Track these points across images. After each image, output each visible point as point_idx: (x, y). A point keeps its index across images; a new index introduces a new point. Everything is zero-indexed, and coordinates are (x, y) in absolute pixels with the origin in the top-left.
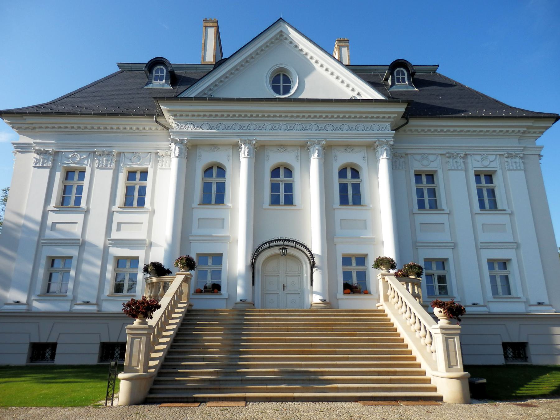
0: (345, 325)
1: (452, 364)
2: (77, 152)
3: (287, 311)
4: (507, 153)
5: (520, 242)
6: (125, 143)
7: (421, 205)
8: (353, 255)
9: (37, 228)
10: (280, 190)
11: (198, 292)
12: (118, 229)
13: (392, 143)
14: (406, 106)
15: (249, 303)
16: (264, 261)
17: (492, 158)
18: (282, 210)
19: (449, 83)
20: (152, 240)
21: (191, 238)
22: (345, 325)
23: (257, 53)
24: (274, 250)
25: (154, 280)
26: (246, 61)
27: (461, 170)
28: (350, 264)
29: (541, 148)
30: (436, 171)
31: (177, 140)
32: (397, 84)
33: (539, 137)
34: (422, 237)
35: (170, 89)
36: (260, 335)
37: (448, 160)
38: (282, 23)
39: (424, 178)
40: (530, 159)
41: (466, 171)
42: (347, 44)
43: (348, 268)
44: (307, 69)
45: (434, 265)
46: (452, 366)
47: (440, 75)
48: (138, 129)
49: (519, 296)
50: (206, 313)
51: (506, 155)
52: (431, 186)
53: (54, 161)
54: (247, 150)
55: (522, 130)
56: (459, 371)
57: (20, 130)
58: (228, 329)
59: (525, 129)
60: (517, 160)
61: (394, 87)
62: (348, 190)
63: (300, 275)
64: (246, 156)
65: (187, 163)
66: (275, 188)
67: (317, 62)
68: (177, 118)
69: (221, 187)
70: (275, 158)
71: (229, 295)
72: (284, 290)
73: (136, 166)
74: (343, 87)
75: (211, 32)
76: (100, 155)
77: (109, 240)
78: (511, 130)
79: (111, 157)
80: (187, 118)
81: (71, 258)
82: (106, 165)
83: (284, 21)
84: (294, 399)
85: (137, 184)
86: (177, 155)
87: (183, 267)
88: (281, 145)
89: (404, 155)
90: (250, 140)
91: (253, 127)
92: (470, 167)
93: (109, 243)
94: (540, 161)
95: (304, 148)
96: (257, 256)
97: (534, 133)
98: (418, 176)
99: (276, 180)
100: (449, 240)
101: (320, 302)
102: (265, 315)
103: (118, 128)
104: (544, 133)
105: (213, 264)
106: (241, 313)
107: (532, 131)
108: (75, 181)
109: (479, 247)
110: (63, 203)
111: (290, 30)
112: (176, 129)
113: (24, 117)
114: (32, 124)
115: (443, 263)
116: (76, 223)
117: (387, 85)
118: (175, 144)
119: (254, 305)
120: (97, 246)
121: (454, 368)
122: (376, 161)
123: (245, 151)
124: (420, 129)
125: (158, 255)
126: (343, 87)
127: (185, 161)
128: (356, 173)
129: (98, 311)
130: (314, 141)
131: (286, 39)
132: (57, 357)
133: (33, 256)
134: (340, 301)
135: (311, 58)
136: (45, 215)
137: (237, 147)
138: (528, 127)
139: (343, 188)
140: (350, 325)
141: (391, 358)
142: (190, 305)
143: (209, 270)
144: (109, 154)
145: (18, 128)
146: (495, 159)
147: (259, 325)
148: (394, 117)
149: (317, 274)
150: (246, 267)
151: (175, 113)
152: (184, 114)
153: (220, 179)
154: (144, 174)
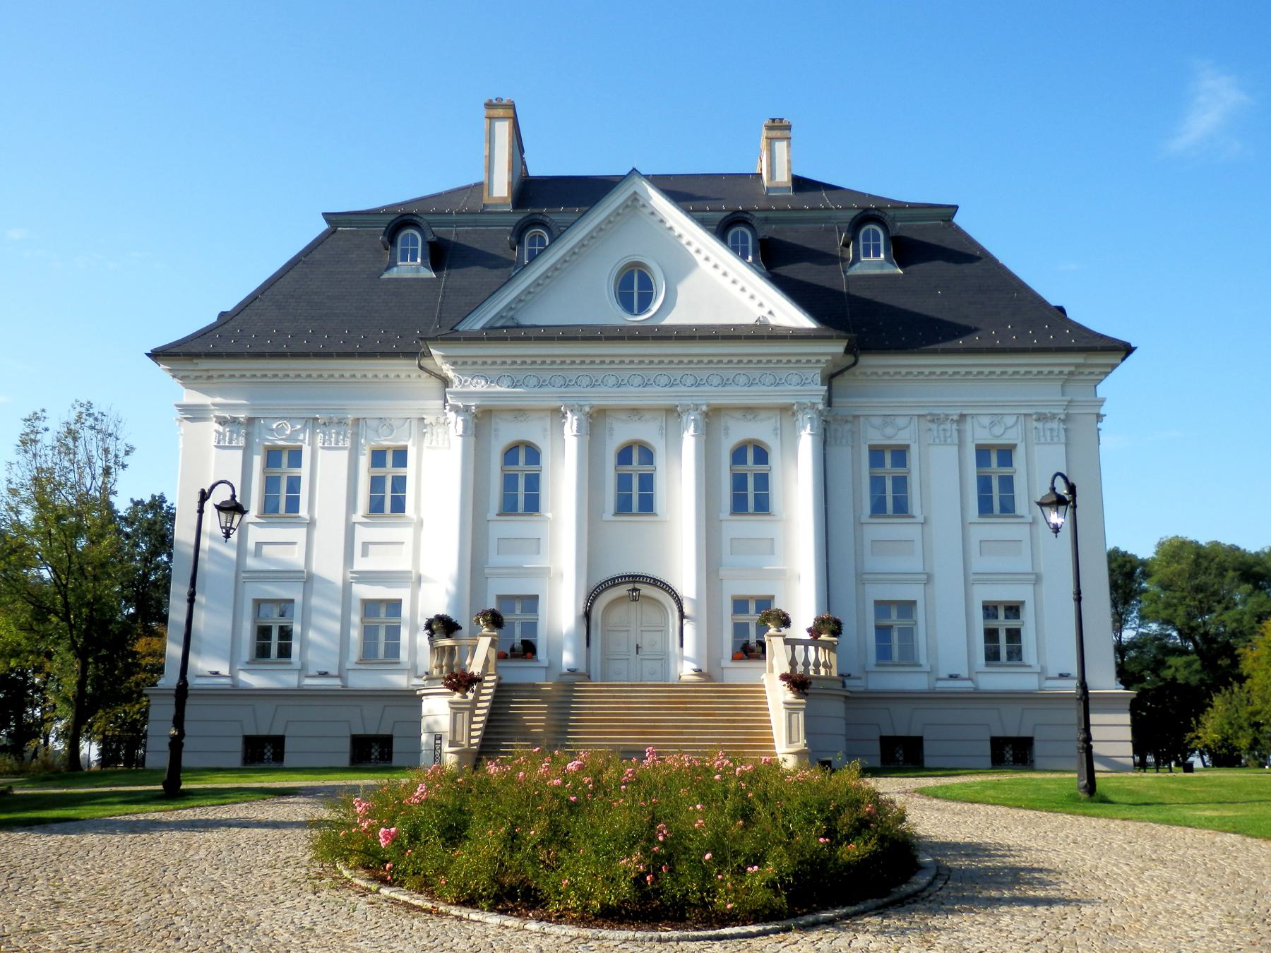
2: (285, 418)
7: (878, 508)
8: (752, 597)
10: (633, 490)
13: (821, 407)
17: (1010, 420)
18: (635, 524)
19: (969, 252)
21: (487, 571)
23: (591, 237)
24: (621, 591)
25: (447, 642)
26: (572, 252)
29: (1103, 400)
30: (908, 446)
32: (863, 259)
34: (874, 563)
35: (431, 279)
40: (1080, 423)
41: (961, 445)
42: (786, 133)
44: (684, 264)
52: (899, 471)
55: (1066, 370)
59: (1073, 369)
60: (1055, 425)
61: (858, 265)
62: (745, 487)
63: (663, 630)
65: (476, 442)
66: (623, 482)
69: (533, 482)
70: (622, 433)
73: (387, 442)
74: (744, 298)
75: (503, 130)
78: (1046, 370)
81: (292, 601)
89: (850, 419)
91: (585, 381)
92: (969, 435)
94: (1100, 425)
95: (672, 412)
96: (595, 598)
97: (1091, 373)
98: (877, 454)
99: (626, 469)
100: (920, 569)
107: (1087, 371)
108: (285, 471)
109: (969, 580)
115: (907, 607)
117: (845, 260)
118: (457, 412)
122: (795, 438)
124: (880, 371)
125: (436, 598)
126: (744, 298)
127: (472, 440)
128: (762, 455)
131: (644, 206)
135: (689, 244)
137: (557, 414)
138: (1077, 366)
139: (739, 482)
142: (500, 678)
144: (341, 422)
145: (182, 378)
150: (577, 618)
152: (470, 361)
153: (532, 469)
154: (401, 456)
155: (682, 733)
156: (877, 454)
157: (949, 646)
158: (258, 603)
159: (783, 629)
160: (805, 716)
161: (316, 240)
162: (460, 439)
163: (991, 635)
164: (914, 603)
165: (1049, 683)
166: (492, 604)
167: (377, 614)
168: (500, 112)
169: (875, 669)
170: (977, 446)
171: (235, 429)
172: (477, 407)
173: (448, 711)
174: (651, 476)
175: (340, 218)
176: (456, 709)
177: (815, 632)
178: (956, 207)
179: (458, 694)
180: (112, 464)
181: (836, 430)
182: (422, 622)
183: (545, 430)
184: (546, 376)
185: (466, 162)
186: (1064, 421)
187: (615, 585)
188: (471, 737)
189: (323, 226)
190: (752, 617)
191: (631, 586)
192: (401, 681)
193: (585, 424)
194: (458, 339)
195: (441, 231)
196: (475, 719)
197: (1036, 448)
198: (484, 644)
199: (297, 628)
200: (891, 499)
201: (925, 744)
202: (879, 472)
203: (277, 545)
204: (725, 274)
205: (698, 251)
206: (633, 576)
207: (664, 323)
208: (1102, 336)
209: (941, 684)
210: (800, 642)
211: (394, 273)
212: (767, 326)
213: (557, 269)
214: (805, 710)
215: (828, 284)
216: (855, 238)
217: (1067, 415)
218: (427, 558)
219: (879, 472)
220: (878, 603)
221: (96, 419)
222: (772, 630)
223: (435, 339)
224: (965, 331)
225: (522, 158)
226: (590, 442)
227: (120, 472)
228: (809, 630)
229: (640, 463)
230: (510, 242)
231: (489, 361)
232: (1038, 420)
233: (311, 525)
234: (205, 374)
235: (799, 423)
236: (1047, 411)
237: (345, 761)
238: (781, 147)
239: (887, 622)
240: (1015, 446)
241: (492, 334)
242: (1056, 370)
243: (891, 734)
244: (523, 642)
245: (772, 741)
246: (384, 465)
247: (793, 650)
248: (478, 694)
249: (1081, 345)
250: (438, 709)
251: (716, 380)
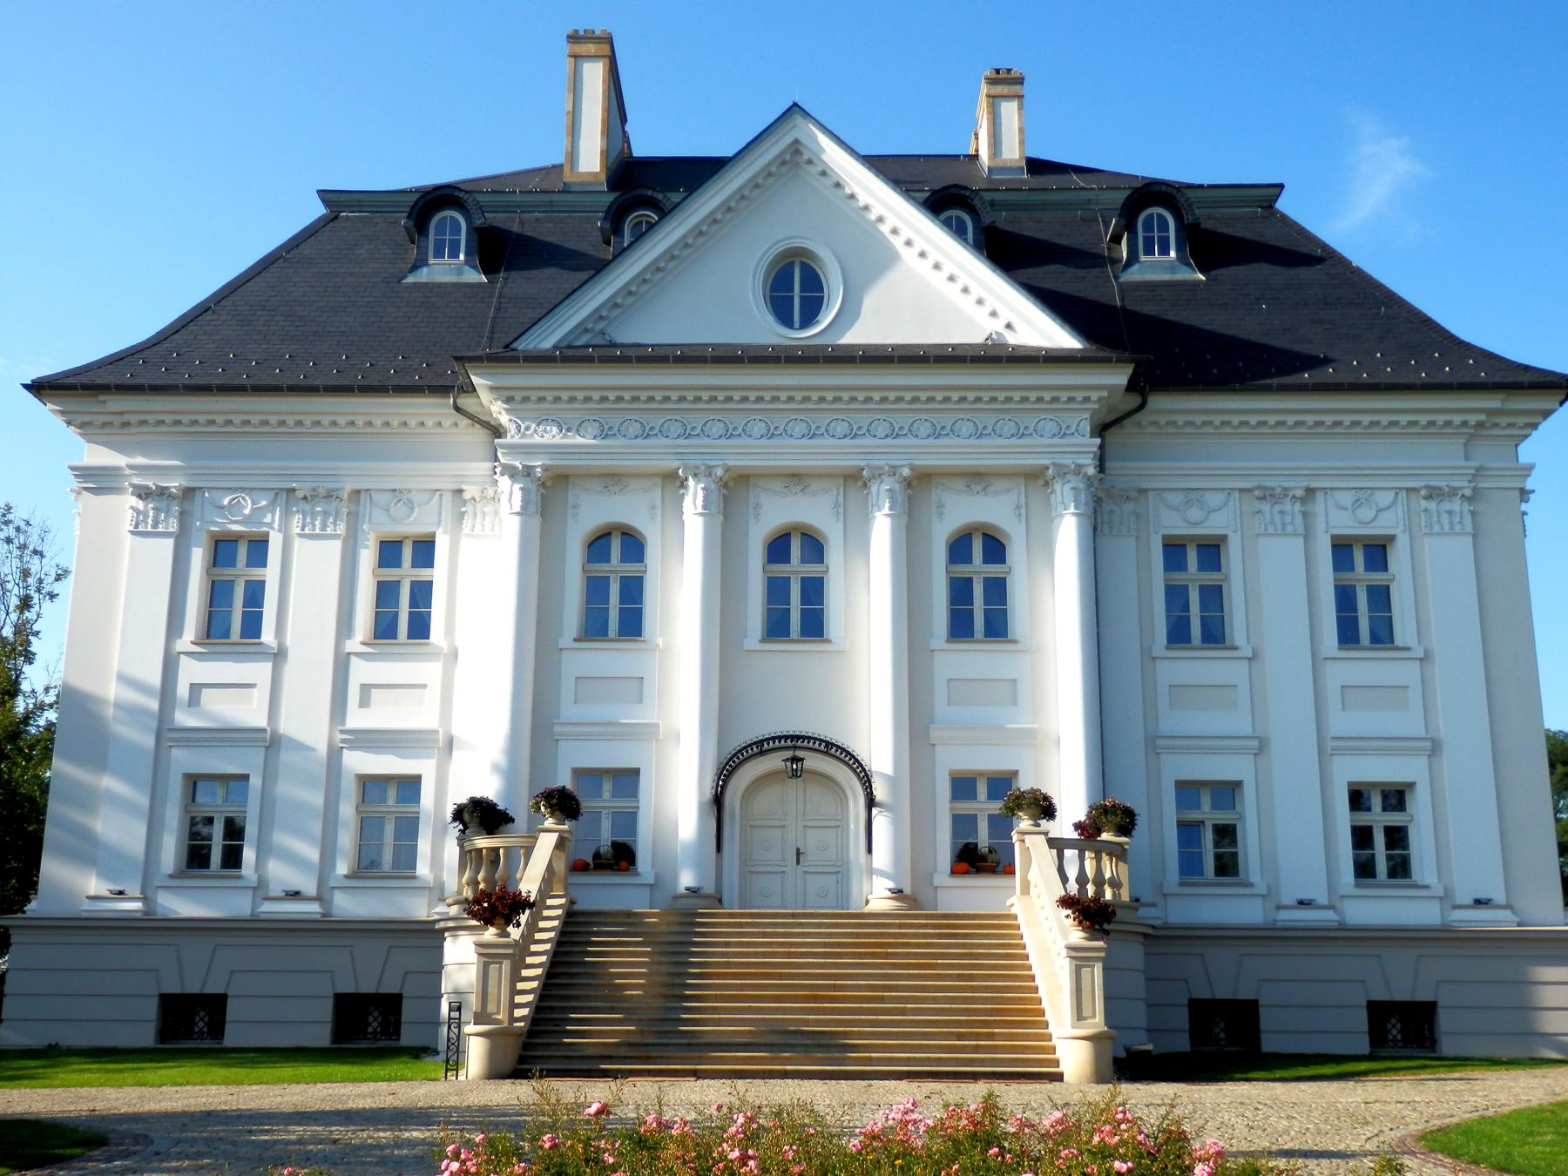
2: (243, 489)
3: (793, 916)
4: (1426, 487)
5: (1442, 734)
7: (1178, 634)
8: (981, 774)
9: (154, 705)
10: (794, 607)
11: (578, 867)
13: (1091, 471)
14: (1130, 371)
16: (747, 789)
17: (1385, 498)
18: (795, 656)
19: (1305, 250)
20: (454, 732)
21: (556, 729)
24: (772, 762)
25: (483, 842)
27: (1295, 535)
29: (1530, 468)
30: (1224, 538)
31: (515, 468)
32: (1143, 258)
33: (1527, 436)
34: (1173, 721)
35: (480, 285)
36: (729, 965)
37: (1260, 505)
38: (799, 120)
39: (1192, 557)
40: (1491, 507)
41: (1308, 536)
42: (1016, 89)
43: (966, 807)
44: (877, 257)
45: (1206, 800)
47: (1284, 219)
48: (405, 424)
49: (1427, 881)
51: (1423, 492)
52: (1211, 577)
53: (184, 517)
54: (700, 494)
55: (1473, 419)
56: (1097, 1023)
57: (87, 429)
59: (1483, 417)
60: (1456, 505)
61: (1136, 267)
62: (972, 599)
63: (840, 826)
64: (700, 510)
65: (542, 525)
66: (776, 590)
67: (895, 231)
68: (515, 406)
69: (633, 590)
70: (776, 512)
71: (657, 876)
72: (798, 862)
73: (414, 526)
74: (966, 304)
75: (594, 75)
76: (305, 498)
77: (342, 732)
78: (1440, 419)
79: (335, 504)
80: (541, 406)
83: (806, 114)
84: (785, 1075)
86: (518, 509)
87: (552, 814)
88: (794, 475)
89: (1134, 494)
90: (710, 467)
91: (717, 429)
92: (1320, 525)
93: (343, 741)
94: (1524, 507)
95: (854, 479)
96: (731, 773)
98: (1174, 550)
99: (780, 569)
100: (1248, 731)
101: (889, 894)
103: (352, 423)
104: (1541, 427)
106: (688, 920)
107: (1504, 421)
108: (242, 571)
110: (214, 631)
111: (824, 140)
113: (102, 398)
114: (121, 413)
115: (1228, 791)
116: (252, 686)
117: (1115, 261)
118: (512, 477)
119: (720, 901)
123: (695, 495)
124: (1181, 419)
125: (476, 776)
126: (966, 304)
127: (537, 521)
128: (996, 549)
130: (880, 468)
131: (810, 162)
132: (229, 1030)
133: (149, 781)
134: (940, 891)
136: (170, 665)
137: (673, 481)
138: (1490, 412)
139: (960, 591)
142: (572, 902)
144: (329, 495)
145: (82, 426)
146: (1394, 502)
147: (727, 945)
148: (1100, 399)
149: (881, 822)
150: (701, 804)
151: (510, 393)
152: (534, 395)
153: (631, 568)
154: (425, 550)
155: (882, 1000)
156: (1174, 550)
157: (1297, 852)
158: (193, 782)
159: (1043, 822)
160: (1104, 969)
161: (306, 229)
162: (517, 519)
163: (1362, 837)
164: (1239, 784)
165: (1458, 915)
166: (564, 780)
168: (591, 48)
169: (1176, 889)
170: (1334, 537)
171: (163, 505)
173: (474, 958)
175: (343, 198)
176: (488, 955)
177: (1089, 830)
178: (1281, 186)
179: (492, 930)
180: (32, 593)
181: (1111, 512)
182: (450, 810)
184: (656, 421)
185: (539, 130)
186: (1469, 499)
187: (762, 753)
189: (319, 210)
190: (984, 807)
191: (789, 754)
192: (420, 909)
193: (715, 497)
194: (515, 360)
195: (497, 219)
197: (1426, 540)
199: (251, 831)
200: (1198, 619)
201: (1263, 1012)
202: (1178, 578)
203: (233, 694)
204: (937, 267)
205: (895, 231)
206: (792, 737)
207: (842, 342)
208: (1527, 368)
209: (1284, 915)
210: (1069, 844)
211: (423, 276)
212: (1005, 346)
213: (673, 257)
215: (1091, 294)
216: (1130, 227)
217: (1475, 489)
218: (460, 714)
219: (1178, 578)
221: (18, 529)
222: (1025, 823)
223: (477, 359)
224: (1312, 362)
225: (624, 132)
227: (47, 604)
229: (803, 561)
230: (601, 229)
231: (565, 395)
232: (1428, 498)
233: (278, 656)
234: (117, 419)
235: (1056, 498)
236: (1270, 483)
238: (1009, 109)
239: (1193, 816)
240: (1392, 538)
241: (569, 355)
242: (1457, 419)
243: (1207, 995)
244: (615, 845)
247: (1061, 857)
248: (532, 927)
249: (1497, 379)
250: (461, 957)
251: (924, 429)
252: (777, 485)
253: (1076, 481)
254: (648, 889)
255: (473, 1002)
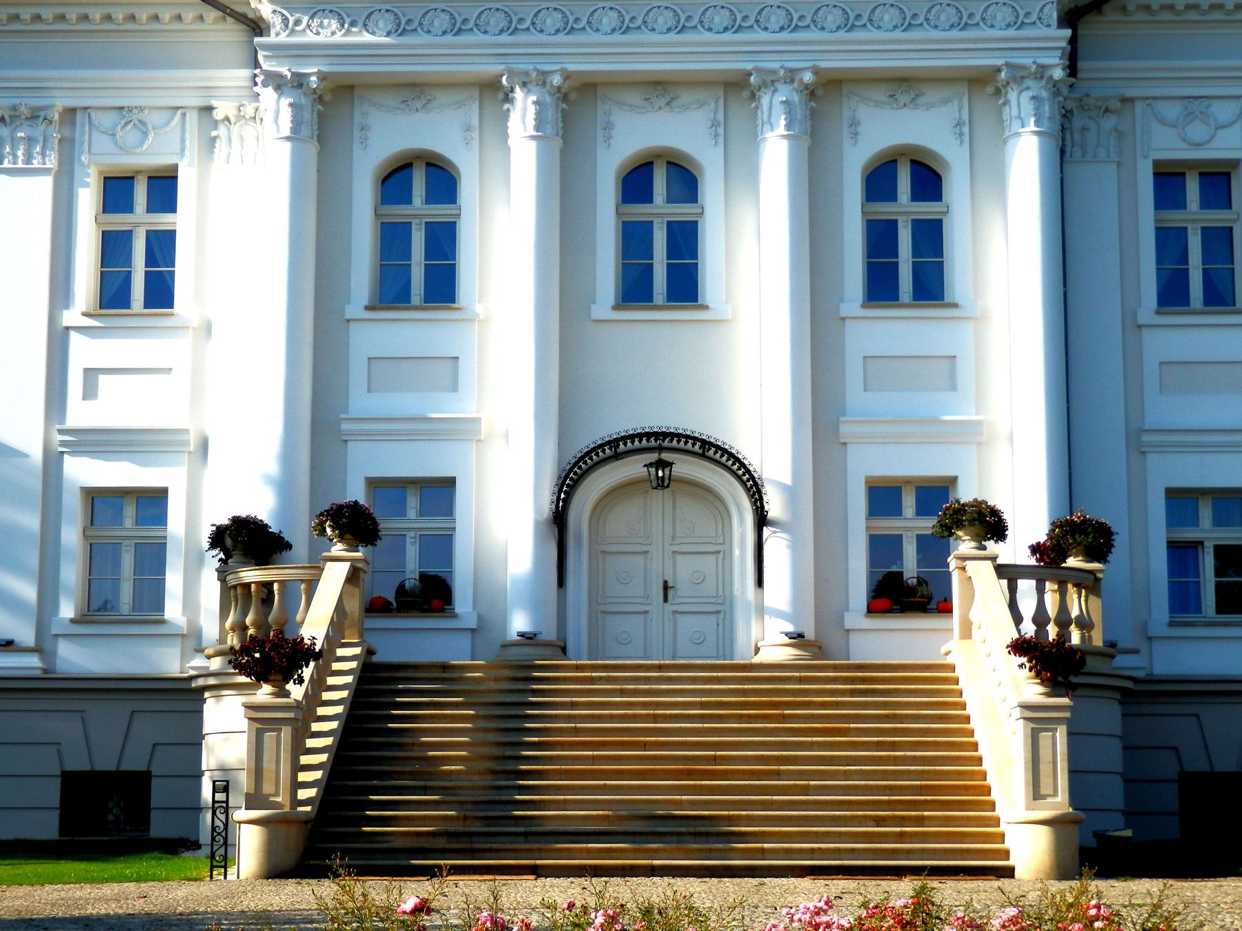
0: (824, 705)
1: (1043, 792)
3: (660, 668)
6: (90, 73)
7: (1172, 293)
8: (908, 481)
10: (661, 267)
11: (376, 607)
12: (90, 392)
13: (1058, 74)
15: (548, 644)
18: (657, 328)
21: (345, 426)
22: (824, 705)
24: (631, 469)
25: (251, 575)
28: (897, 511)
34: (1168, 410)
43: (888, 525)
45: (1206, 512)
46: (1044, 797)
50: (419, 675)
54: (532, 110)
58: (486, 717)
63: (721, 551)
65: (321, 155)
66: (634, 239)
69: (443, 240)
71: (480, 618)
72: (666, 600)
73: (151, 154)
77: (61, 432)
79: (42, 128)
82: (28, 160)
85: (138, 225)
87: (342, 538)
88: (657, 83)
93: (63, 444)
95: (737, 89)
96: (576, 483)
98: (1168, 180)
99: (639, 211)
102: (592, 680)
105: (421, 514)
112: (279, 35)
118: (278, 88)
119: (564, 650)
120: (26, 456)
121: (1049, 800)
125: (244, 475)
127: (312, 149)
128: (929, 180)
129: (45, 671)
130: (774, 72)
134: (854, 638)
137: (493, 93)
139: (880, 238)
140: (837, 705)
141: (921, 787)
142: (370, 652)
143: (412, 534)
144: (34, 116)
147: (573, 705)
149: (776, 546)
150: (537, 523)
153: (440, 212)
154: (164, 188)
155: (778, 775)
156: (1168, 180)
159: (990, 544)
160: (1070, 734)
166: (356, 493)
167: (118, 520)
172: (323, 77)
174: (694, 224)
176: (261, 721)
179: (267, 688)
181: (1084, 129)
183: (468, 129)
187: (617, 456)
188: (296, 785)
190: (912, 525)
191: (653, 457)
192: (170, 662)
193: (550, 113)
196: (305, 760)
198: (334, 577)
214: (1068, 722)
219: (1174, 218)
220: (1174, 495)
222: (965, 546)
226: (563, 152)
228: (1036, 549)
229: (670, 200)
235: (1011, 111)
237: (47, 827)
239: (1189, 534)
244: (424, 577)
245: (987, 790)
246: (128, 208)
247: (1013, 590)
248: (319, 684)
250: (226, 730)
252: (634, 98)
253: (1037, 87)
254: (469, 634)
255: (243, 781)
